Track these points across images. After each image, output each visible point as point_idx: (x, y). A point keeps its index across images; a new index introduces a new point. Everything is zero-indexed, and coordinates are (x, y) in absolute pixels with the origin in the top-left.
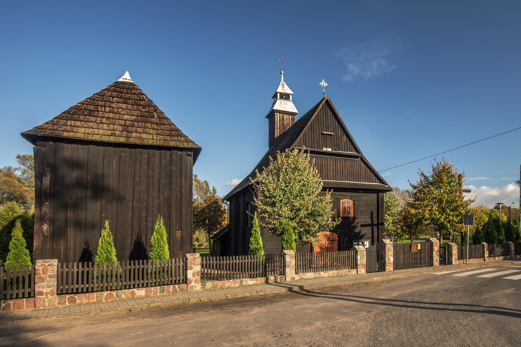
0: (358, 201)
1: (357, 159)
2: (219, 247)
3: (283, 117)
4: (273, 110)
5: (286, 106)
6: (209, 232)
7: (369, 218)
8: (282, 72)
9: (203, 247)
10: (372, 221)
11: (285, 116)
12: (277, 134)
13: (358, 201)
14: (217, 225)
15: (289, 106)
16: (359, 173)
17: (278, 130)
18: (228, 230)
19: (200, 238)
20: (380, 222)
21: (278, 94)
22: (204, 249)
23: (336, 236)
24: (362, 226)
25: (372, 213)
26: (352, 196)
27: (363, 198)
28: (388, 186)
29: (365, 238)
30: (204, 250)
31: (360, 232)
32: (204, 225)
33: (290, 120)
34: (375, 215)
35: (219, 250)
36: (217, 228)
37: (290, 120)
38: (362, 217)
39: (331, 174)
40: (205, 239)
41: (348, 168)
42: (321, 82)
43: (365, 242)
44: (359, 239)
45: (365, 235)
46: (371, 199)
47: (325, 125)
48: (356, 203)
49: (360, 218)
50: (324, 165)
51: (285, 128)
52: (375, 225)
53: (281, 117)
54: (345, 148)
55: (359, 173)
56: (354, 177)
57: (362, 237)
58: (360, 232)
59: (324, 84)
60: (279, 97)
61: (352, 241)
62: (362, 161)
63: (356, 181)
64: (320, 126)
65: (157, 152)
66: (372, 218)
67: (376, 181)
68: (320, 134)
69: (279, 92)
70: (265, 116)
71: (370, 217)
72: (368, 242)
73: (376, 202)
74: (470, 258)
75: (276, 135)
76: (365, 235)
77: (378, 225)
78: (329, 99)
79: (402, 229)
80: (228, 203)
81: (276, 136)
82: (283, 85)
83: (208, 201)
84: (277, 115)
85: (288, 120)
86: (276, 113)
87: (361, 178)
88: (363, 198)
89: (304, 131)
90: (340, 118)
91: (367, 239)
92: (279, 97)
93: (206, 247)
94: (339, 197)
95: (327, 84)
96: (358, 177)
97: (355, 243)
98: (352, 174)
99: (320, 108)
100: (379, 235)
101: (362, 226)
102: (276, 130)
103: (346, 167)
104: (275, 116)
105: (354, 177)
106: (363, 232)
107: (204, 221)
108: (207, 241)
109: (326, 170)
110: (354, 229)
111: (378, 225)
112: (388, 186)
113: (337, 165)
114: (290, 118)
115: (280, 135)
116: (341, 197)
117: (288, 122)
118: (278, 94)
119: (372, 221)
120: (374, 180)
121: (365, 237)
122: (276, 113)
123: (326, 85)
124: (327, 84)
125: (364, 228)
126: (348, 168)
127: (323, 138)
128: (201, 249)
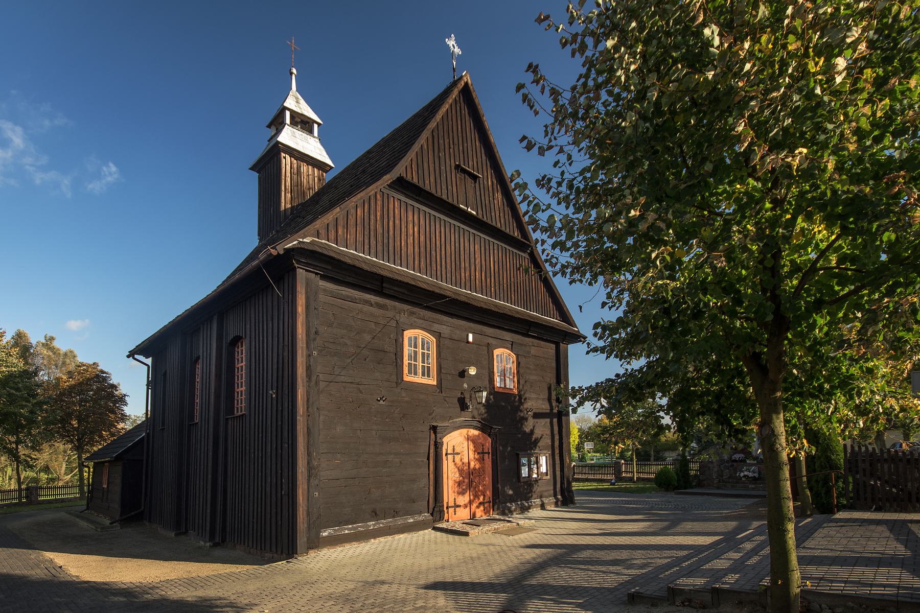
2: (118, 480)
3: (299, 168)
4: (278, 142)
5: (305, 144)
6: (79, 448)
7: (543, 399)
8: (294, 71)
9: (61, 484)
10: (552, 409)
11: (304, 168)
12: (286, 201)
15: (311, 146)
16: (528, 289)
17: (289, 195)
18: (148, 434)
19: (54, 465)
21: (288, 113)
22: (63, 487)
26: (515, 342)
27: (533, 351)
28: (576, 329)
30: (64, 491)
32: (66, 435)
33: (316, 179)
35: (117, 489)
36: (101, 436)
37: (316, 179)
39: (477, 277)
40: (64, 466)
45: (541, 438)
48: (522, 360)
50: (462, 249)
51: (304, 194)
53: (295, 166)
54: (502, 222)
55: (528, 289)
58: (532, 432)
60: (288, 121)
61: (518, 455)
64: (452, 146)
68: (453, 168)
69: (289, 109)
70: (250, 167)
71: (546, 396)
75: (283, 205)
76: (541, 438)
80: (149, 361)
81: (283, 208)
82: (297, 98)
83: (79, 373)
84: (285, 158)
85: (310, 177)
86: (283, 155)
88: (533, 351)
89: (416, 147)
92: (288, 121)
93: (67, 483)
94: (491, 341)
99: (454, 96)
102: (283, 193)
103: (505, 267)
104: (280, 161)
107: (65, 421)
108: (70, 470)
109: (467, 265)
112: (576, 329)
113: (488, 258)
114: (316, 174)
115: (292, 207)
117: (311, 182)
118: (288, 113)
119: (552, 409)
122: (283, 155)
127: (457, 177)
128: (55, 488)
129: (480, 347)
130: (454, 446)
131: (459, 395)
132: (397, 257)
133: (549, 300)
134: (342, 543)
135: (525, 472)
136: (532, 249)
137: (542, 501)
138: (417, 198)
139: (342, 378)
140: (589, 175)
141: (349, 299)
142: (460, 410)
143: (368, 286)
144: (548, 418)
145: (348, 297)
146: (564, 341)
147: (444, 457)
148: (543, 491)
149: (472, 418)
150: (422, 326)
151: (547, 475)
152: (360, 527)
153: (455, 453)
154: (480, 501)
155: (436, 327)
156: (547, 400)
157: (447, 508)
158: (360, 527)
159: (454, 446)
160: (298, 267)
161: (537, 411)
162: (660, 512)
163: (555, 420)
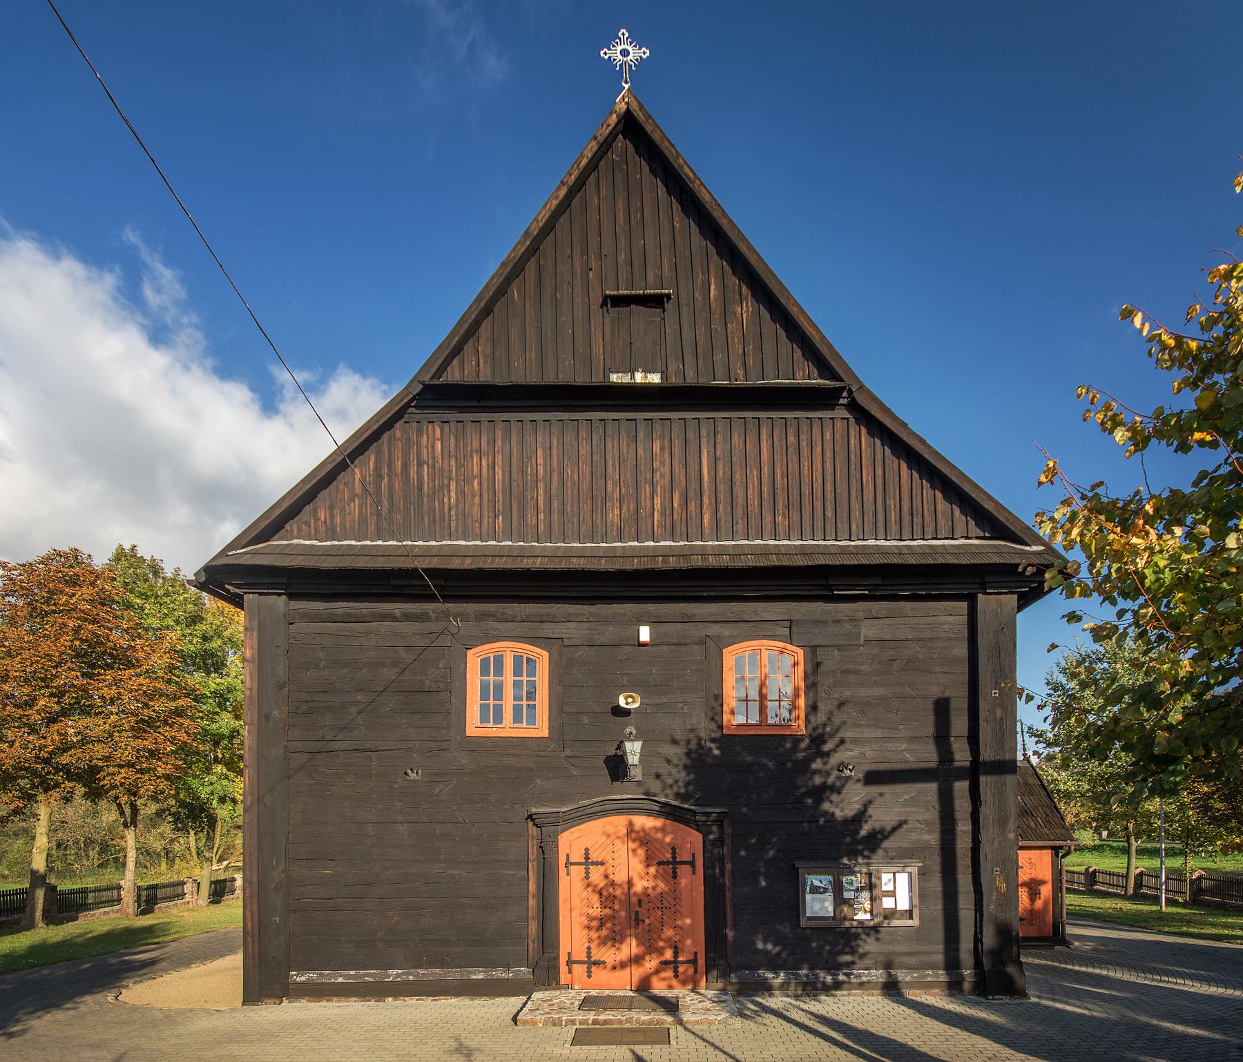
0: (840, 648)
1: (826, 414)
10: (945, 754)
13: (840, 648)
14: (817, 946)
20: (987, 754)
23: (692, 842)
24: (873, 778)
25: (942, 708)
27: (868, 630)
29: (886, 850)
31: (860, 817)
34: (959, 725)
38: (869, 733)
41: (765, 471)
42: (608, 43)
43: (886, 877)
44: (853, 854)
45: (894, 829)
46: (928, 635)
47: (622, 256)
48: (830, 660)
49: (855, 741)
52: (960, 774)
55: (842, 488)
56: (806, 516)
57: (874, 841)
58: (860, 817)
59: (625, 53)
62: (858, 421)
63: (819, 533)
64: (594, 263)
65: (1126, 865)
66: (942, 738)
67: (960, 530)
71: (930, 729)
72: (903, 879)
73: (962, 651)
74: (344, 459)
77: (975, 771)
78: (641, 106)
79: (1206, 809)
87: (856, 513)
88: (868, 630)
90: (707, 197)
91: (900, 858)
94: (715, 629)
95: (645, 53)
96: (830, 514)
97: (815, 880)
98: (795, 498)
100: (984, 835)
101: (873, 778)
105: (806, 516)
106: (880, 817)
110: (819, 800)
111: (975, 771)
116: (726, 631)
119: (945, 754)
120: (943, 522)
121: (885, 844)
123: (636, 54)
124: (645, 53)
125: (886, 789)
126: (765, 471)
129: (684, 648)
130: (587, 850)
131: (612, 751)
132: (440, 527)
133: (927, 492)
134: (69, 998)
135: (819, 906)
136: (850, 392)
137: (890, 975)
138: (482, 404)
139: (343, 746)
140: (627, 99)
141: (353, 619)
142: (609, 779)
143: (375, 591)
144: (934, 781)
145: (349, 615)
146: (985, 589)
147: (562, 871)
148: (894, 953)
149: (645, 794)
150: (514, 634)
151: (911, 917)
152: (370, 975)
153: (587, 862)
154: (663, 959)
155: (549, 630)
156: (931, 740)
157: (570, 962)
158: (370, 975)
159: (587, 850)
160: (245, 593)
161: (874, 767)
162: (877, 1056)
163: (961, 787)
